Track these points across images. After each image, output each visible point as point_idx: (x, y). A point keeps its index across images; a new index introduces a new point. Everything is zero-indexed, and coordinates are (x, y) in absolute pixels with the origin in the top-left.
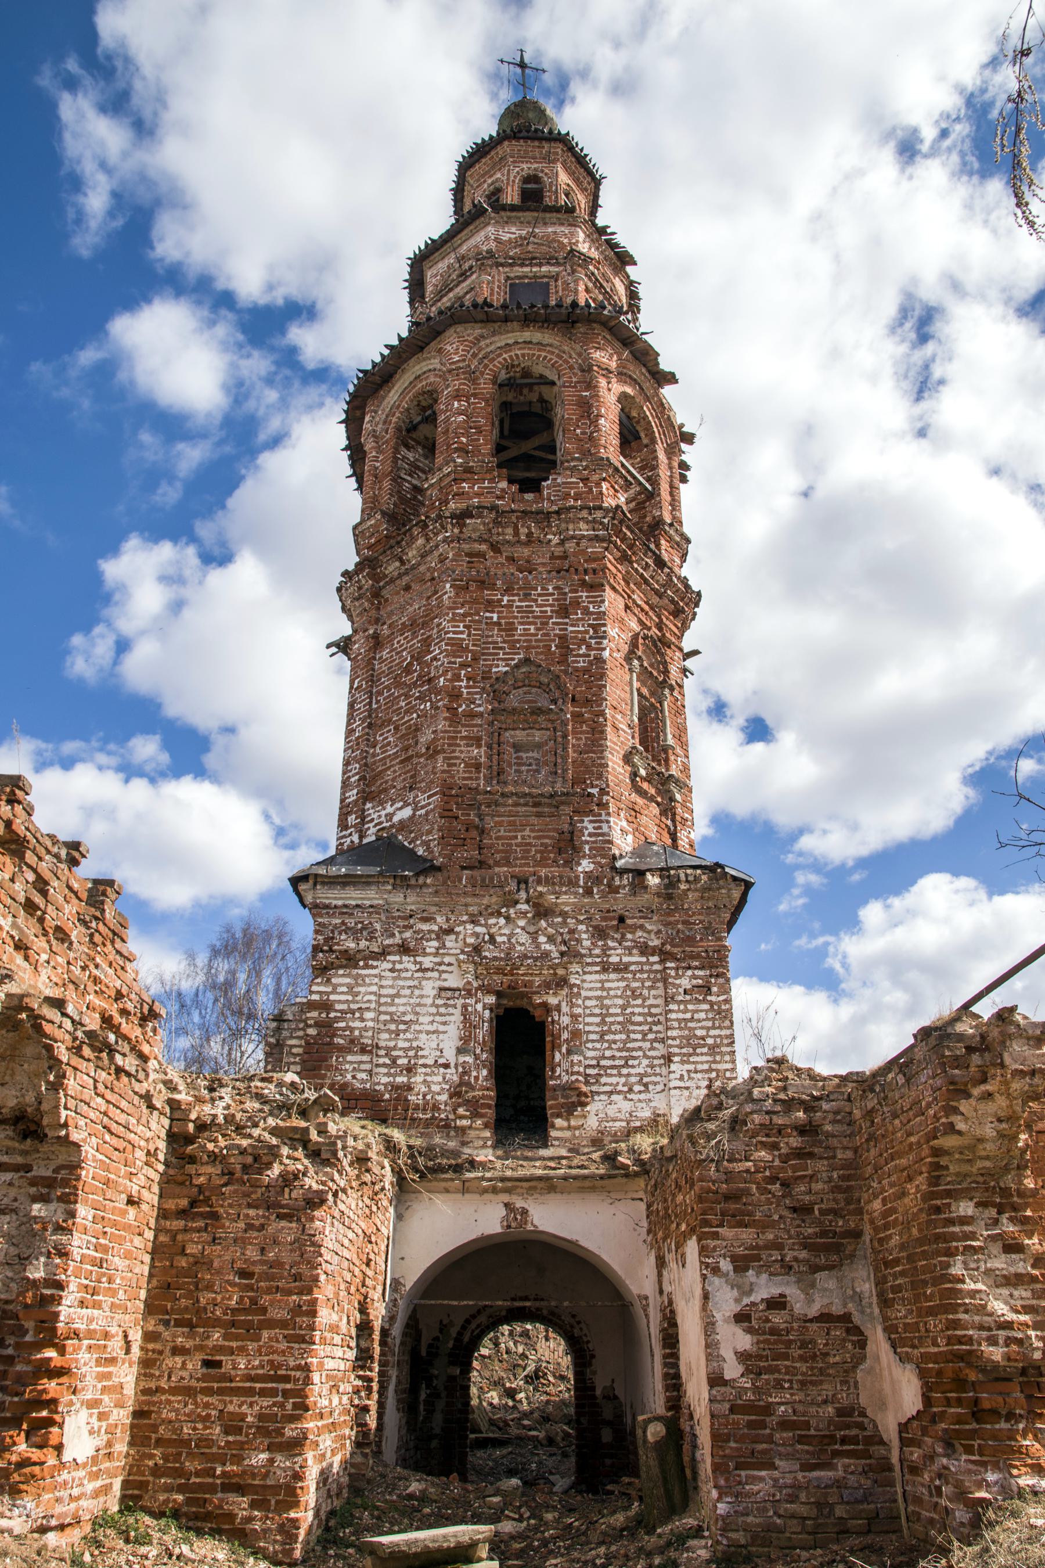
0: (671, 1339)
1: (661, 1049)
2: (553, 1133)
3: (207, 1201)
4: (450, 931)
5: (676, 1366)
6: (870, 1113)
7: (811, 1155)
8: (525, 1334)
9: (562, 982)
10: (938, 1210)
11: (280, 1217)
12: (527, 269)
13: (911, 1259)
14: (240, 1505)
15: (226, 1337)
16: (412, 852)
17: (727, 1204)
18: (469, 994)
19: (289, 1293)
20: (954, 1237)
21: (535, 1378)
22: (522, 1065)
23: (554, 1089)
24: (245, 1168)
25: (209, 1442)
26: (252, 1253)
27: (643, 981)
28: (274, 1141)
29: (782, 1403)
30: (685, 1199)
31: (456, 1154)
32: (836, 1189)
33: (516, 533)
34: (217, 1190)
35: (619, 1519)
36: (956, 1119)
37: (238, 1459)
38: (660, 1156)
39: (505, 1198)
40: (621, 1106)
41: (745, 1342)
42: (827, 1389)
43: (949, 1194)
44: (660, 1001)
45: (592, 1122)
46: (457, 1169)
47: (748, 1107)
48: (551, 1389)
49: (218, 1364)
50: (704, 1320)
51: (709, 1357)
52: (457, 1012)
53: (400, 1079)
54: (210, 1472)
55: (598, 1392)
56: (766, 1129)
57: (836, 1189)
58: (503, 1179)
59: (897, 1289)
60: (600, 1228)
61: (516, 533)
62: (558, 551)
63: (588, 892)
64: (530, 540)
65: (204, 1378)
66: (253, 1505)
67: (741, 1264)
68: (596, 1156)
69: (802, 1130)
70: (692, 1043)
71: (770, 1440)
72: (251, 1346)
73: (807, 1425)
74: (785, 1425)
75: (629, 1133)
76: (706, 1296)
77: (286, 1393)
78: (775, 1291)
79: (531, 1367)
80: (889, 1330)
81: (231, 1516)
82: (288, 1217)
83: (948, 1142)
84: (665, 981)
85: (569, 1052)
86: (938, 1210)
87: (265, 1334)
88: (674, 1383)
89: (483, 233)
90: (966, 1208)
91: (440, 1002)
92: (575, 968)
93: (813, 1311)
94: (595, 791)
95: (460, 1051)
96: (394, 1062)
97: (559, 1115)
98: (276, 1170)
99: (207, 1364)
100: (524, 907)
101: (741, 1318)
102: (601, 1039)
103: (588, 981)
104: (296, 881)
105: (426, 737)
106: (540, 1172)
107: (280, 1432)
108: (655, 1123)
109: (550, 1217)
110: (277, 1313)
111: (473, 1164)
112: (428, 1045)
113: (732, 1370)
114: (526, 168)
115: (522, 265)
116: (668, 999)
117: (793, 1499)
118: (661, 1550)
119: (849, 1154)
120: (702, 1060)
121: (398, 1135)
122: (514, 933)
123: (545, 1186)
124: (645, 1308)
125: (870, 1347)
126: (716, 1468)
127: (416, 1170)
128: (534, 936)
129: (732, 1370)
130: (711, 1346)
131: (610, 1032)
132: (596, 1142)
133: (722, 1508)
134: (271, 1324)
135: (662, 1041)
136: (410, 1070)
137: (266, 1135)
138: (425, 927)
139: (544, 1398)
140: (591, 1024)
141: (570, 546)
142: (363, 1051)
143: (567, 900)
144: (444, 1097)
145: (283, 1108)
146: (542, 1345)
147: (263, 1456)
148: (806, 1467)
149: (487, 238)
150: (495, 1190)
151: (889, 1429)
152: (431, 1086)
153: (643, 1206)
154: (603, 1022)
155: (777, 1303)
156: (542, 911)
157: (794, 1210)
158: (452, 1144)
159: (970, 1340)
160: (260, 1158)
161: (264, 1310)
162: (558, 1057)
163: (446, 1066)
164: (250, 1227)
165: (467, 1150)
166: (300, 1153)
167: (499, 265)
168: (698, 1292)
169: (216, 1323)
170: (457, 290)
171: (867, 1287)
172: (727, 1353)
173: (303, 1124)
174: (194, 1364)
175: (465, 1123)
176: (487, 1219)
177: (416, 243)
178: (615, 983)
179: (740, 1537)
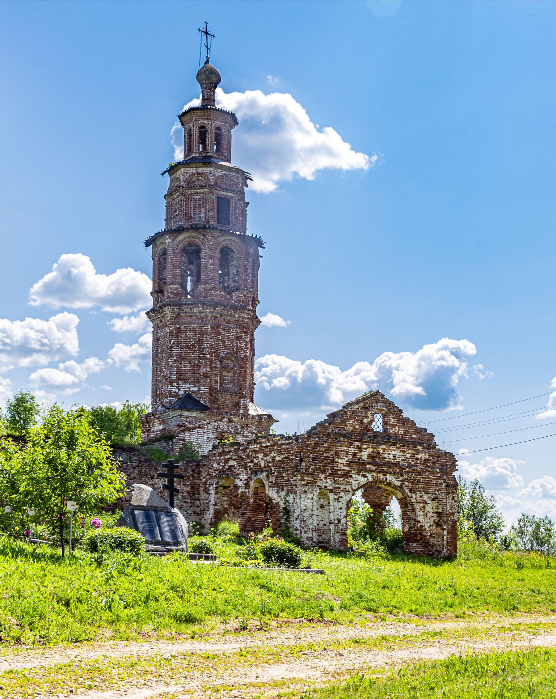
4: (209, 423)
12: (224, 193)
16: (199, 401)
33: (228, 312)
61: (228, 312)
62: (237, 319)
63: (242, 418)
64: (231, 315)
94: (244, 392)
100: (226, 420)
104: (450, 558)
105: (202, 371)
122: (223, 425)
128: (228, 426)
138: (204, 422)
141: (241, 319)
143: (237, 420)
156: (230, 421)
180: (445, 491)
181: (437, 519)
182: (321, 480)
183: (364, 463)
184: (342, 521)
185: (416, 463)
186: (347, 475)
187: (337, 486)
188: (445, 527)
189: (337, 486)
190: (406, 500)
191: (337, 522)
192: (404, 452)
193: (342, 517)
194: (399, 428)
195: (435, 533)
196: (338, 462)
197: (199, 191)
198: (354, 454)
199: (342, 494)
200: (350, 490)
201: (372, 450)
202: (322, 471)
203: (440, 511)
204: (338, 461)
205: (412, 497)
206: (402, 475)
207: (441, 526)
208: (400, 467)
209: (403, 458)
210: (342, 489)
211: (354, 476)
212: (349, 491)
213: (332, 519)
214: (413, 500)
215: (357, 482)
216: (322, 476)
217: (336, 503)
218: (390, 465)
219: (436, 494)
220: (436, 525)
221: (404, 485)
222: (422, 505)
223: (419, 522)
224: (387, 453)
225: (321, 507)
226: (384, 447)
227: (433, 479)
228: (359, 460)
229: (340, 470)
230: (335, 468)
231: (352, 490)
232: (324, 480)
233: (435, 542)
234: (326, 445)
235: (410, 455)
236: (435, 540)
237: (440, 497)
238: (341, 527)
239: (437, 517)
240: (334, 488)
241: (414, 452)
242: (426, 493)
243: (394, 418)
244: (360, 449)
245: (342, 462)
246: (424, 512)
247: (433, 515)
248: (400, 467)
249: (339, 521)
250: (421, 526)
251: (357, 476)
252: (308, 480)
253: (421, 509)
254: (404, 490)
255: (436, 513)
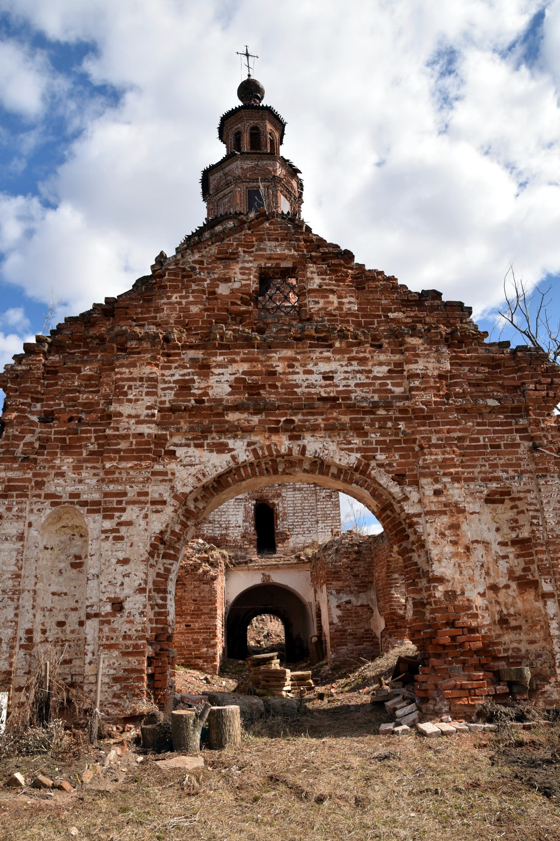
0: (319, 615)
1: (315, 518)
2: (278, 549)
3: (181, 580)
5: (321, 623)
6: (375, 548)
7: (359, 560)
8: (262, 620)
9: (279, 495)
10: (389, 576)
11: (204, 584)
13: (383, 589)
14: (200, 662)
15: (191, 618)
17: (334, 575)
18: (246, 501)
19: (209, 605)
20: (393, 583)
21: (268, 636)
22: (266, 528)
23: (278, 533)
24: (192, 570)
25: (190, 646)
26: (197, 594)
27: (308, 494)
28: (199, 561)
29: (350, 629)
30: (322, 573)
31: (245, 557)
32: (366, 569)
34: (184, 577)
35: (305, 664)
36: (392, 554)
37: (198, 650)
38: (314, 556)
39: (262, 572)
40: (301, 538)
41: (339, 613)
42: (362, 625)
43: (392, 572)
44: (314, 501)
45: (291, 545)
46: (246, 563)
47: (341, 547)
48: (274, 640)
49: (190, 626)
50: (327, 607)
51: (329, 617)
52: (242, 507)
53: (224, 532)
54: (191, 654)
55: (294, 637)
56: (346, 553)
57: (366, 569)
58: (262, 566)
59: (381, 597)
60: (295, 581)
65: (186, 629)
66: (204, 662)
67: (338, 592)
68: (293, 556)
69: (356, 552)
70: (326, 516)
71: (346, 638)
72: (199, 620)
73: (356, 634)
74: (350, 634)
75: (304, 548)
76: (328, 601)
77: (210, 632)
78: (348, 599)
79: (265, 633)
80: (379, 608)
81: (198, 665)
82: (206, 584)
83: (391, 559)
84: (316, 494)
85: (282, 520)
86: (389, 576)
87: (203, 617)
88: (320, 628)
89: (235, 164)
90: (396, 576)
91: (236, 504)
92: (284, 490)
93: (359, 604)
95: (244, 521)
96: (221, 526)
97: (280, 543)
98: (201, 571)
99: (186, 626)
101: (338, 606)
102: (294, 515)
103: (288, 494)
106: (274, 563)
107: (209, 643)
108: (313, 544)
109: (278, 578)
110: (205, 611)
111: (251, 561)
112: (233, 519)
113: (336, 621)
114: (252, 123)
115: (253, 182)
116: (317, 501)
117: (352, 653)
118: (316, 668)
119: (370, 559)
120: (329, 522)
121: (225, 552)
123: (276, 567)
124: (311, 606)
125: (374, 613)
126: (331, 647)
127: (232, 564)
129: (336, 621)
130: (330, 614)
131: (297, 513)
132: (293, 552)
133: (333, 656)
134: (204, 614)
135: (315, 515)
136: (227, 528)
137: (197, 560)
139: (271, 643)
140: (290, 510)
142: (210, 522)
144: (239, 538)
145: (199, 551)
146: (269, 624)
147: (205, 649)
148: (356, 645)
149: (237, 167)
150: (258, 569)
151: (378, 634)
152: (235, 534)
153: (309, 573)
154: (294, 509)
155: (348, 602)
157: (354, 576)
158: (243, 554)
159: (395, 609)
160: (196, 567)
161: (202, 610)
162: (278, 522)
163: (239, 527)
164: (195, 587)
165: (248, 556)
166: (207, 564)
167: (243, 182)
168: (326, 600)
169: (188, 614)
170: (225, 191)
171: (374, 597)
172: (334, 616)
173: (206, 556)
174: (183, 626)
175: (247, 546)
176: (256, 579)
177: (206, 165)
178: (298, 495)
179: (338, 663)
180: (532, 467)
181: (519, 565)
182: (62, 475)
183: (219, 409)
184: (127, 605)
185: (411, 389)
186: (155, 450)
187: (112, 488)
188: (547, 587)
189: (112, 488)
190: (393, 511)
191: (108, 608)
192: (363, 361)
193: (127, 591)
194: (340, 297)
195: (517, 614)
196: (120, 414)
197: (226, 191)
198: (184, 387)
199: (131, 513)
200: (167, 496)
201: (245, 367)
202: (67, 449)
203: (525, 533)
204: (120, 409)
205: (406, 499)
206: (360, 431)
207: (535, 584)
208: (352, 408)
209: (362, 379)
210: (132, 493)
211: (180, 452)
212: (164, 503)
213: (95, 600)
214: (410, 509)
215: (193, 470)
216: (66, 463)
217: (107, 545)
218: (311, 404)
219: (498, 479)
220: (520, 586)
221: (373, 463)
222: (445, 520)
223: (441, 580)
224: (300, 370)
225: (74, 566)
226: (289, 353)
227: (479, 432)
228: (200, 401)
229: (125, 437)
230: (109, 432)
231: (176, 497)
232: (70, 474)
233: (524, 647)
234: (87, 370)
235: (385, 369)
236: (523, 637)
237: (516, 486)
238: (125, 627)
239: (518, 556)
240: (106, 495)
241: (397, 357)
242: (456, 479)
243: (320, 273)
244: (204, 368)
245: (135, 413)
246: (455, 543)
247: (502, 551)
248: (352, 408)
249: (118, 606)
250: (451, 595)
251: (192, 450)
252: (10, 480)
253: (443, 535)
254: (374, 480)
255: (514, 543)
